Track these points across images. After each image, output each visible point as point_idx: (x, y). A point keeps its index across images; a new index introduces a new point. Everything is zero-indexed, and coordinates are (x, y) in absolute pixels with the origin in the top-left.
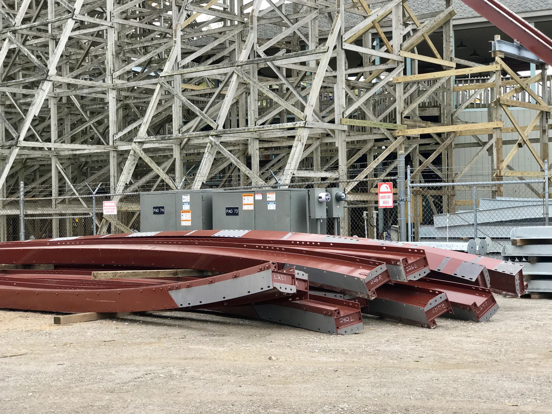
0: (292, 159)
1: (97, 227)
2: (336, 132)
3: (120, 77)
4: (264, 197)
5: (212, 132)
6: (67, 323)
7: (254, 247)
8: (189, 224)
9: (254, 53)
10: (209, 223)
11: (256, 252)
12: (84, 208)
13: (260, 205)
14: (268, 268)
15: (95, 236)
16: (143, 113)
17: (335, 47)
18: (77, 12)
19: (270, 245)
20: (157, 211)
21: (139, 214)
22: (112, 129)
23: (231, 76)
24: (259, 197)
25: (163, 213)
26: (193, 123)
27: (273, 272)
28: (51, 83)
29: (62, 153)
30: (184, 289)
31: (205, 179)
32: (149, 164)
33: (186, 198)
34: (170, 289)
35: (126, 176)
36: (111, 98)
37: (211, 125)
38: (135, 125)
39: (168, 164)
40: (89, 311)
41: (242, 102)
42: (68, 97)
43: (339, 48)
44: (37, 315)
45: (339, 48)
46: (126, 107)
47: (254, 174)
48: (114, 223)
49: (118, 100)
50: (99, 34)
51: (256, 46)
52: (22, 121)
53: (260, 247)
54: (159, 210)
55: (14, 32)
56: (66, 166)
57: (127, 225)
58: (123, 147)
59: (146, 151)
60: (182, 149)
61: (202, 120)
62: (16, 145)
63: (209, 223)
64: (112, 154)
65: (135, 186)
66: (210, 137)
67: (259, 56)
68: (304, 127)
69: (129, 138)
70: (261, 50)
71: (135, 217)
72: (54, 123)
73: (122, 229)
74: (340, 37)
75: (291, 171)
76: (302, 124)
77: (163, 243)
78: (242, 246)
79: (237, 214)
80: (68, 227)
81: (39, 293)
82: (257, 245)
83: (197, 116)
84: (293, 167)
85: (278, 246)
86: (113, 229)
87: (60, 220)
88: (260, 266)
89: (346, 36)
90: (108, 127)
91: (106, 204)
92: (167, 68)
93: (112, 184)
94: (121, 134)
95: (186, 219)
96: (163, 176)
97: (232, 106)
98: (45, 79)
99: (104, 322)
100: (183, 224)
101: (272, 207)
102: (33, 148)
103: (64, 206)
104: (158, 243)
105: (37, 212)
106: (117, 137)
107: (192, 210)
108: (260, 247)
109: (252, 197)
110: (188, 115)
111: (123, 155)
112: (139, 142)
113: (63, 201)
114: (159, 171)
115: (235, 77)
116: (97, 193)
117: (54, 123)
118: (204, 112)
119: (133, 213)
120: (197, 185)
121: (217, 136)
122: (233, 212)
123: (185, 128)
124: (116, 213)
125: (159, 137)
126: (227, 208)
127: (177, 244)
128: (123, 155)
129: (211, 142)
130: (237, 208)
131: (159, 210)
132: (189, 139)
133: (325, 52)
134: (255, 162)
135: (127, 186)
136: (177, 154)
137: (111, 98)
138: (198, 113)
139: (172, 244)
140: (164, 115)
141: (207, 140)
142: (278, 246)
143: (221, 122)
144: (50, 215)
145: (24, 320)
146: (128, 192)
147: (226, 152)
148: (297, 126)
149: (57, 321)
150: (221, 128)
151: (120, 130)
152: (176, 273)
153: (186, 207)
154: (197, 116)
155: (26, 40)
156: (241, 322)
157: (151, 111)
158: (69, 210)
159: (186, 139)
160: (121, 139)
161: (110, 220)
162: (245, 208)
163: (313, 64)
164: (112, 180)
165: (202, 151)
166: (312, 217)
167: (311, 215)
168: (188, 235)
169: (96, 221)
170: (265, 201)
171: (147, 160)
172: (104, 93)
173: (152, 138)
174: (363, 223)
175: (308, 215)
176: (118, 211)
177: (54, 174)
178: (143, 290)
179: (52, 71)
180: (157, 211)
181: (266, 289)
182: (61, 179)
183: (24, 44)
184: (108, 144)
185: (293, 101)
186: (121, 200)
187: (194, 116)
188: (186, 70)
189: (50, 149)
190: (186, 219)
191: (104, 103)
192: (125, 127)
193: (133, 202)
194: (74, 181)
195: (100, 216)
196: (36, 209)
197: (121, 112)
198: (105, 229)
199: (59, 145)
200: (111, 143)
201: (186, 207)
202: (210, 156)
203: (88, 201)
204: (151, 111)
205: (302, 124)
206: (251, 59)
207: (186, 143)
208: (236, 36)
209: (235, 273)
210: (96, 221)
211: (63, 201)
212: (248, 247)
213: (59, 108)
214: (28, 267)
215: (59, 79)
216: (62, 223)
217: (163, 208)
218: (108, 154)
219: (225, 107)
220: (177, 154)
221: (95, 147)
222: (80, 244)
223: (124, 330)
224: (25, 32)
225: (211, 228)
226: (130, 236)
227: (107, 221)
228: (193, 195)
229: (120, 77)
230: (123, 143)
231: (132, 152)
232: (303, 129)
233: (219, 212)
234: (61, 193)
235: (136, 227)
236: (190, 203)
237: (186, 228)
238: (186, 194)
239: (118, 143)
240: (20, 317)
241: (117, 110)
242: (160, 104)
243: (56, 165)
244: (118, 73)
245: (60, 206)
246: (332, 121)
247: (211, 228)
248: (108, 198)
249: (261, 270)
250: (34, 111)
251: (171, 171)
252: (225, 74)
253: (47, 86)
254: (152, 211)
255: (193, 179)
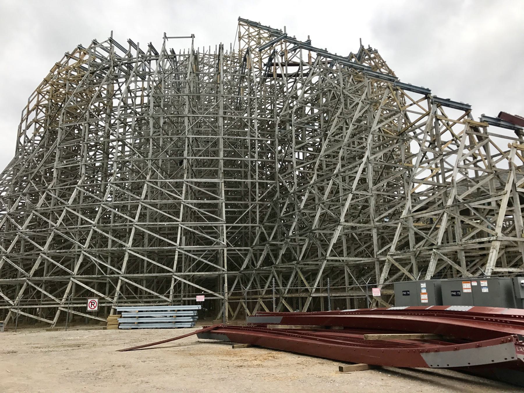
0: (491, 260)
1: (370, 303)
2: (519, 243)
3: (377, 222)
4: (479, 284)
5: (434, 247)
6: (349, 370)
7: (482, 319)
8: (426, 301)
9: (455, 200)
10: (440, 301)
11: (485, 324)
12: (362, 293)
13: (476, 289)
14: (511, 341)
15: (368, 309)
16: (392, 240)
17: (511, 191)
18: (353, 190)
19: (497, 318)
20: (405, 293)
21: (394, 296)
22: (376, 249)
23: (443, 214)
24: (475, 284)
25: (409, 295)
26: (422, 243)
27: (515, 344)
28: (341, 226)
29: (350, 263)
30: (433, 353)
31: (433, 273)
32: (398, 267)
33: (423, 285)
34: (421, 352)
35: (385, 274)
36: (374, 233)
37: (434, 243)
38: (388, 246)
39: (408, 267)
40: (363, 363)
41: (451, 229)
42: (352, 235)
43: (514, 191)
44: (329, 362)
45: (514, 191)
46: (383, 238)
47: (463, 270)
48: (380, 301)
49: (378, 235)
50: (367, 201)
51: (457, 197)
52: (328, 245)
53: (487, 320)
54: (406, 293)
55: (323, 203)
56: (352, 270)
57: (387, 302)
58: (383, 259)
59: (396, 260)
60: (416, 258)
61: (427, 240)
62: (325, 259)
63: (440, 301)
64: (376, 263)
65: (391, 280)
66: (434, 250)
67: (459, 201)
68: (497, 240)
69: (385, 253)
70: (460, 198)
71: (392, 297)
72: (344, 247)
73: (384, 304)
74: (514, 185)
75: (491, 267)
76: (495, 238)
77: (411, 315)
78: (472, 318)
79: (460, 295)
80: (356, 303)
81: (331, 347)
82: (485, 318)
83: (424, 238)
84: (492, 264)
85: (499, 319)
86: (379, 304)
87: (351, 299)
88: (502, 339)
89: (518, 184)
90: (373, 250)
91: (374, 290)
92: (404, 213)
93: (377, 278)
94: (380, 252)
95: (424, 298)
96: (407, 273)
97: (445, 232)
98: (339, 224)
99: (373, 372)
100: (423, 301)
101: (485, 290)
102: (336, 261)
103: (352, 291)
104: (408, 315)
105: (337, 295)
106: (379, 253)
107: (428, 293)
108: (487, 320)
109: (470, 284)
110: (418, 239)
111: (382, 263)
112: (391, 255)
113: (352, 289)
114: (404, 271)
115: (445, 215)
116: (368, 284)
117: (344, 247)
118: (428, 236)
119: (390, 296)
120: (428, 277)
121: (437, 249)
122: (457, 293)
123: (417, 246)
124: (380, 295)
125: (402, 251)
126: (452, 291)
127: (421, 315)
128: (382, 263)
129: (434, 253)
130: (459, 291)
131: (406, 293)
132: (420, 253)
133: (504, 194)
134: (464, 263)
135: (386, 280)
136: (413, 261)
137: (374, 233)
138: (425, 237)
139: (418, 315)
140: (403, 242)
141: (431, 252)
142: (499, 319)
143: (440, 241)
144: (345, 296)
145: (320, 366)
146: (387, 283)
147: (445, 258)
148: (491, 239)
149: (341, 369)
150: (439, 244)
151: (380, 249)
152: (423, 337)
153: (424, 291)
154: (424, 238)
155: (330, 207)
156: (481, 381)
157: (396, 239)
158: (355, 294)
159: (418, 252)
160: (380, 254)
161: (377, 299)
162: (465, 291)
163: (494, 204)
164: (377, 276)
165: (428, 259)
166: (518, 297)
167: (517, 296)
168: (427, 309)
169: (369, 299)
170: (479, 287)
171: (396, 264)
172: (369, 230)
173: (399, 252)
174: (54, 296)
175: (514, 296)
176: (381, 294)
177: (346, 275)
178: (400, 350)
179: (342, 219)
180: (405, 293)
181: (509, 359)
182: (350, 278)
183: (329, 209)
184: (374, 257)
185: (486, 225)
186: (383, 288)
187: (423, 238)
188: (415, 214)
189: (343, 260)
190: (424, 298)
191: (371, 237)
192: (382, 247)
193: (390, 289)
194: (358, 278)
195: (371, 297)
196: (337, 293)
197: (380, 240)
198: (374, 305)
199: (347, 258)
200: (375, 257)
201: (424, 291)
202: (434, 261)
203: (365, 288)
204: (396, 239)
205: (495, 238)
206: (455, 204)
207: (419, 254)
208: (442, 195)
209: (477, 343)
210: (369, 299)
211: (352, 289)
212: (477, 319)
213: (347, 241)
214: (328, 328)
215: (346, 224)
216: (352, 300)
217: (409, 291)
218: (373, 263)
219: (441, 232)
220: (413, 261)
221: (366, 259)
222: (358, 314)
223: (387, 382)
224: (329, 203)
225: (441, 304)
226: (389, 309)
227: (375, 300)
228: (427, 282)
229: (377, 222)
230: (382, 256)
231: (387, 261)
232: (496, 242)
233: (446, 294)
234: (351, 284)
235: (393, 303)
236: (427, 288)
237: (425, 304)
238: (423, 282)
239: (379, 257)
240: (319, 363)
241: (378, 239)
242: (400, 235)
243: (347, 270)
244: (377, 219)
245: (350, 292)
246: (515, 236)
247: (441, 304)
248: (376, 287)
249: (503, 342)
250: (334, 241)
251: (411, 271)
252: (439, 214)
253: (340, 228)
254: (402, 293)
255: (425, 274)
